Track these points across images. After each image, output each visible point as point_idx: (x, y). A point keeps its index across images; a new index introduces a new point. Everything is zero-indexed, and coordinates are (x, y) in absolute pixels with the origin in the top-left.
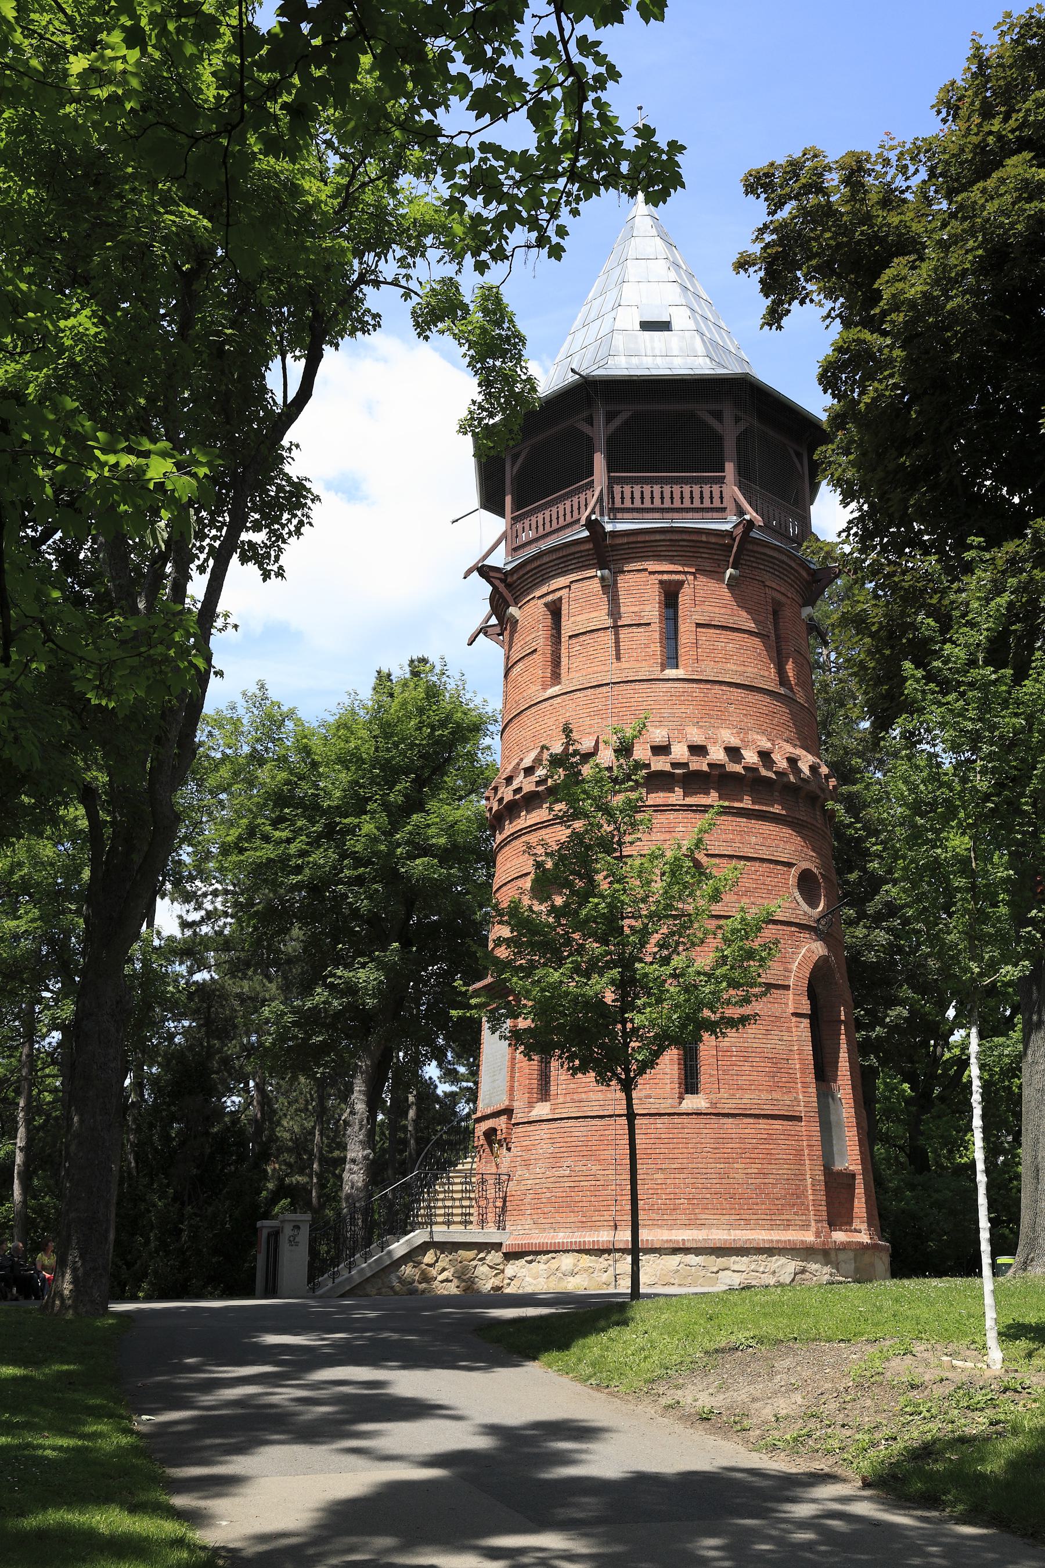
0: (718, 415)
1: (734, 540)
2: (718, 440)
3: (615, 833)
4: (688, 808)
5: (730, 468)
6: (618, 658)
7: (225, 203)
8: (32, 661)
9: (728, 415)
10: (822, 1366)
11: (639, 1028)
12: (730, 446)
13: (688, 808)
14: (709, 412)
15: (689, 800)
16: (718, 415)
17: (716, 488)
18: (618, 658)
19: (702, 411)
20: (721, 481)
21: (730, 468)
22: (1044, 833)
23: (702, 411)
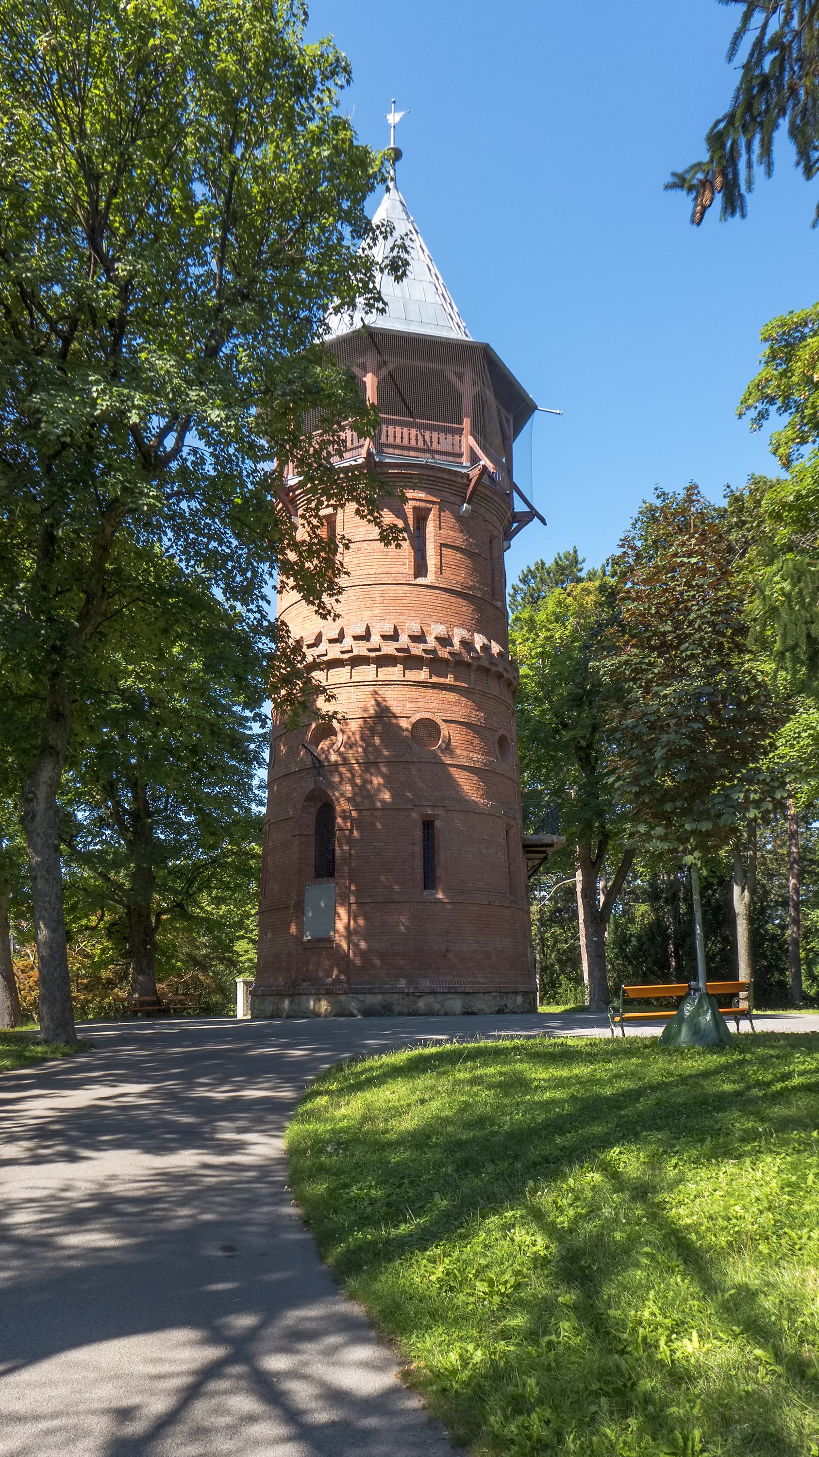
0: (460, 376)
1: (470, 481)
2: (457, 398)
3: (168, 178)
4: (435, 686)
5: (467, 423)
6: (428, 825)
7: (164, 800)
8: (377, 809)
9: (469, 376)
10: (114, 853)
11: (129, 282)
12: (467, 403)
13: (435, 686)
14: (456, 373)
15: (435, 679)
16: (460, 376)
17: (457, 437)
18: (428, 825)
19: (450, 372)
20: (460, 432)
21: (467, 423)
22: (816, 149)
23: (450, 372)
